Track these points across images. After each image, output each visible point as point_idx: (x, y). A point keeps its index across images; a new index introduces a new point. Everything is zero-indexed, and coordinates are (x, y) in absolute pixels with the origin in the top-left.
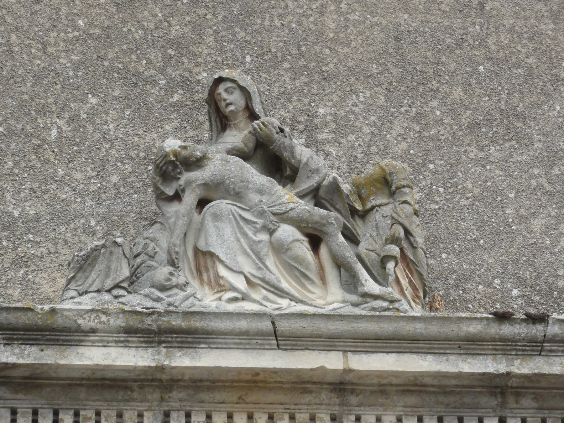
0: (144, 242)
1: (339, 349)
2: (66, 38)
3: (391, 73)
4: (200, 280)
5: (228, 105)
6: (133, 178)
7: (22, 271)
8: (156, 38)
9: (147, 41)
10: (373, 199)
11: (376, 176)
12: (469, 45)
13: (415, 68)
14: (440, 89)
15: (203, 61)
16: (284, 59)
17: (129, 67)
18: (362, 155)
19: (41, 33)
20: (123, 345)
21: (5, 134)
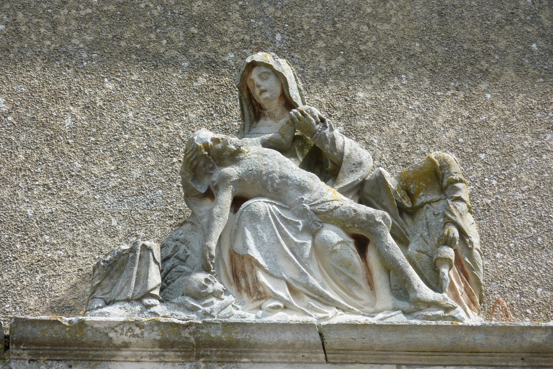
0: (174, 244)
1: (392, 362)
2: (77, 15)
3: (436, 52)
4: (237, 286)
5: (262, 92)
6: (156, 172)
7: (38, 277)
8: (176, 15)
9: (167, 18)
10: (423, 196)
11: (426, 170)
12: (520, 20)
13: (462, 46)
14: (490, 70)
15: (229, 41)
16: (318, 37)
17: (148, 47)
18: (407, 144)
19: (50, 11)
20: (158, 360)
21: (14, 124)
